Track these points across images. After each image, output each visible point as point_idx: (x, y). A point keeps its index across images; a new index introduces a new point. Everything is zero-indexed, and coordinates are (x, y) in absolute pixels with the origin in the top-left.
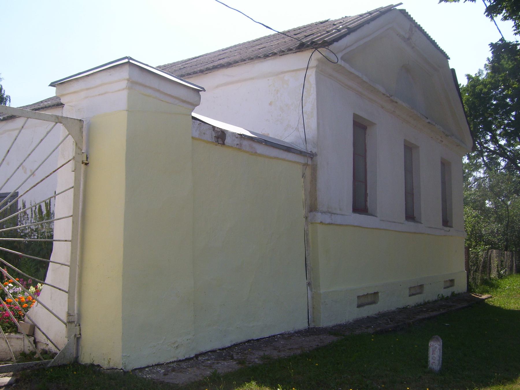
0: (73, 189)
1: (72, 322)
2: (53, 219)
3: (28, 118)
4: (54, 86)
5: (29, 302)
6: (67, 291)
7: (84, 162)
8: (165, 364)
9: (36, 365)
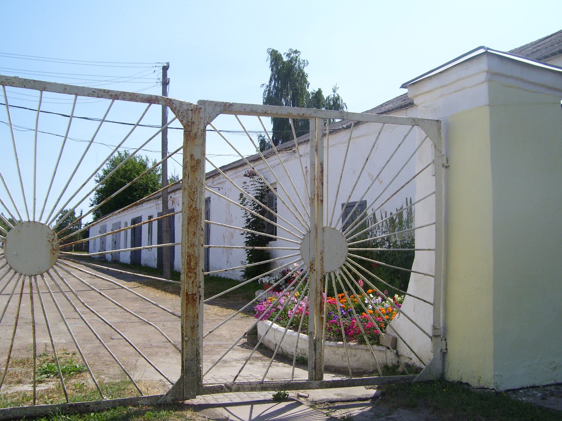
0: (434, 195)
1: (438, 336)
2: (413, 228)
3: (384, 123)
4: (406, 88)
5: (390, 314)
6: (432, 302)
7: (444, 165)
8: (541, 386)
9: (401, 379)
